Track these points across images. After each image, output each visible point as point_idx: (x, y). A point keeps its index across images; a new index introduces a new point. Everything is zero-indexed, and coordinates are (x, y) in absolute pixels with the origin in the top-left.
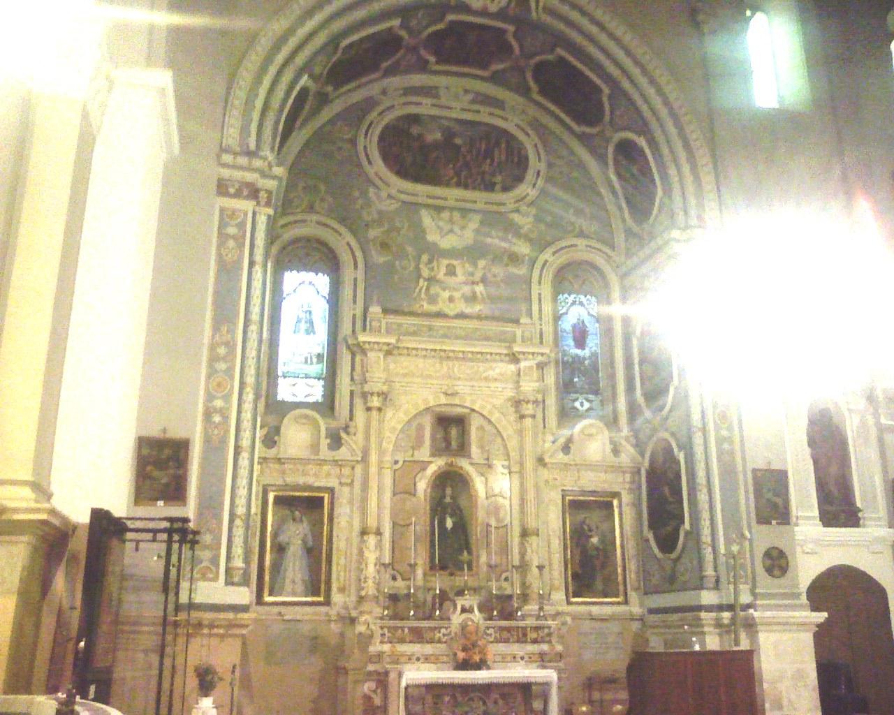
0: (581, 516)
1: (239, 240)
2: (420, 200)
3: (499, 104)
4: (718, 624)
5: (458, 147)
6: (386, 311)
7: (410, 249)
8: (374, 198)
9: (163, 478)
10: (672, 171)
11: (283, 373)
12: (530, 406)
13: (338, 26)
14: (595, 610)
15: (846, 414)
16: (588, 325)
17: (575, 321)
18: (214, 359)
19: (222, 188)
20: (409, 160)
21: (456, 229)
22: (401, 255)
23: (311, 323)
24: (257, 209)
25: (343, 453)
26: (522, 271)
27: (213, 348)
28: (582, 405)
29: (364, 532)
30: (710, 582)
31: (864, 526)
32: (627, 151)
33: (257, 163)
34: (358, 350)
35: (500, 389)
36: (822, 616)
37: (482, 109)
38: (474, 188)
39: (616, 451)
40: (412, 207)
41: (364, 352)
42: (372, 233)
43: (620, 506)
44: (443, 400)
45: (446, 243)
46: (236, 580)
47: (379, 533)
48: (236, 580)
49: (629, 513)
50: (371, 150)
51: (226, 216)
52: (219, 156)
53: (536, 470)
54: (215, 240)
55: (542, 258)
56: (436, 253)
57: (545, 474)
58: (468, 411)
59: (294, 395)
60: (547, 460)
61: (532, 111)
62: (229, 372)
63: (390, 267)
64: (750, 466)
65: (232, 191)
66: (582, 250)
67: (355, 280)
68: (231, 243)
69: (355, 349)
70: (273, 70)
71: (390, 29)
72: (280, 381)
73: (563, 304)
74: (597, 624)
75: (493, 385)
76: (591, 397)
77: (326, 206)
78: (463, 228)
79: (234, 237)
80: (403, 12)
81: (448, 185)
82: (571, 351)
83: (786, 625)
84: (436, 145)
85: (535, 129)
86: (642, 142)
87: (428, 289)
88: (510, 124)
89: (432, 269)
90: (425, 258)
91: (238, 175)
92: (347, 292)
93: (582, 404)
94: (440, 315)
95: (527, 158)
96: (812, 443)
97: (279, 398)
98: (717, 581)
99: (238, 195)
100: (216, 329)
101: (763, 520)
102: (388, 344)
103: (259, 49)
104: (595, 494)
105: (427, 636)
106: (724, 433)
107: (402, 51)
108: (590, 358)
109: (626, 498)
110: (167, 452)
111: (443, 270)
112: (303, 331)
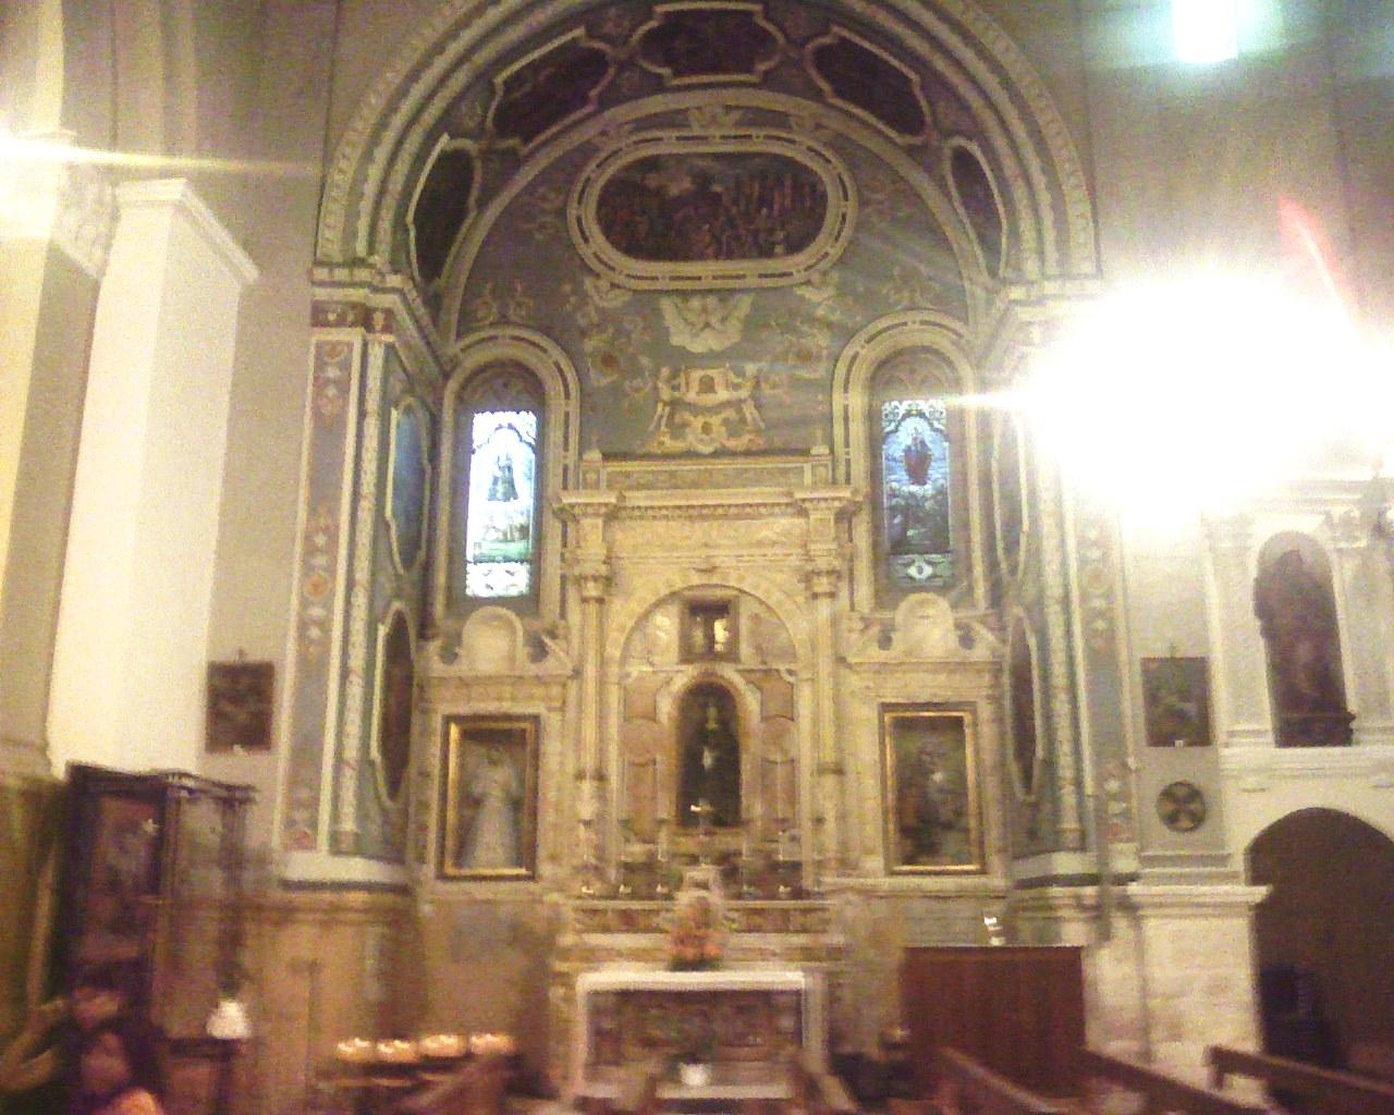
0: (915, 743)
1: (344, 390)
2: (658, 285)
3: (780, 120)
4: (1080, 906)
5: (718, 196)
6: (607, 457)
7: (645, 361)
8: (592, 292)
9: (242, 717)
10: (1019, 192)
11: (475, 557)
12: (824, 580)
13: (482, 57)
14: (929, 883)
15: (1334, 557)
16: (930, 445)
17: (909, 442)
18: (311, 550)
19: (319, 317)
20: (643, 228)
21: (714, 320)
22: (638, 372)
23: (511, 483)
24: (370, 337)
25: (550, 665)
26: (819, 371)
27: (308, 538)
28: (920, 571)
29: (580, 776)
30: (1071, 838)
31: (1358, 743)
32: (963, 160)
33: (363, 274)
34: (567, 516)
35: (781, 557)
36: (1260, 892)
37: (752, 131)
38: (743, 257)
39: (967, 640)
40: (646, 302)
41: (575, 519)
42: (590, 344)
43: (975, 724)
44: (696, 579)
45: (697, 347)
46: (344, 846)
47: (601, 777)
48: (344, 846)
49: (988, 731)
50: (587, 221)
51: (324, 354)
52: (310, 273)
53: (835, 676)
54: (310, 389)
55: (849, 352)
56: (682, 361)
57: (854, 681)
58: (735, 593)
59: (488, 586)
60: (852, 660)
61: (835, 123)
62: (331, 570)
63: (616, 391)
64: (1140, 655)
65: (332, 317)
66: (914, 330)
67: (567, 414)
68: (331, 391)
69: (565, 516)
70: (389, 137)
71: (574, 40)
72: (470, 567)
73: (891, 417)
74: (935, 905)
75: (769, 551)
76: (935, 557)
77: (524, 313)
78: (724, 320)
79: (336, 382)
80: (585, 16)
81: (701, 257)
82: (905, 489)
83: (1198, 907)
84: (681, 201)
85: (838, 151)
86: (974, 149)
87: (671, 415)
88: (797, 149)
89: (675, 388)
90: (665, 371)
91: (339, 294)
92: (555, 436)
93: (920, 570)
94: (691, 454)
95: (824, 196)
96: (1264, 609)
97: (469, 592)
98: (1083, 835)
99: (340, 322)
100: (313, 512)
101: (1160, 737)
102: (606, 505)
103: (366, 112)
104: (941, 708)
105: (642, 921)
106: (1098, 603)
107: (612, 71)
108: (933, 497)
109: (985, 711)
110: (245, 681)
111: (695, 386)
112: (499, 495)
